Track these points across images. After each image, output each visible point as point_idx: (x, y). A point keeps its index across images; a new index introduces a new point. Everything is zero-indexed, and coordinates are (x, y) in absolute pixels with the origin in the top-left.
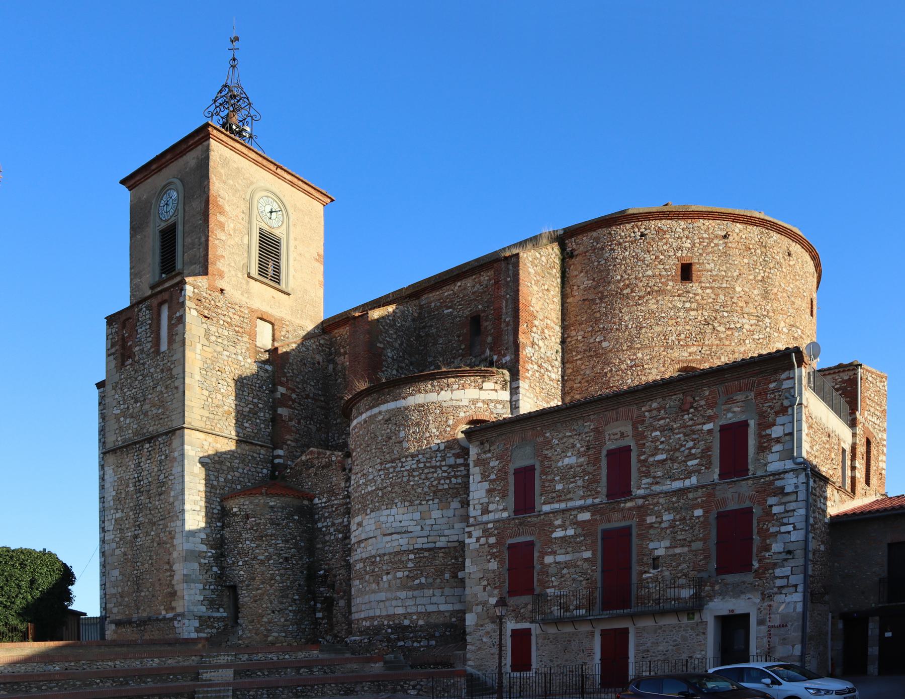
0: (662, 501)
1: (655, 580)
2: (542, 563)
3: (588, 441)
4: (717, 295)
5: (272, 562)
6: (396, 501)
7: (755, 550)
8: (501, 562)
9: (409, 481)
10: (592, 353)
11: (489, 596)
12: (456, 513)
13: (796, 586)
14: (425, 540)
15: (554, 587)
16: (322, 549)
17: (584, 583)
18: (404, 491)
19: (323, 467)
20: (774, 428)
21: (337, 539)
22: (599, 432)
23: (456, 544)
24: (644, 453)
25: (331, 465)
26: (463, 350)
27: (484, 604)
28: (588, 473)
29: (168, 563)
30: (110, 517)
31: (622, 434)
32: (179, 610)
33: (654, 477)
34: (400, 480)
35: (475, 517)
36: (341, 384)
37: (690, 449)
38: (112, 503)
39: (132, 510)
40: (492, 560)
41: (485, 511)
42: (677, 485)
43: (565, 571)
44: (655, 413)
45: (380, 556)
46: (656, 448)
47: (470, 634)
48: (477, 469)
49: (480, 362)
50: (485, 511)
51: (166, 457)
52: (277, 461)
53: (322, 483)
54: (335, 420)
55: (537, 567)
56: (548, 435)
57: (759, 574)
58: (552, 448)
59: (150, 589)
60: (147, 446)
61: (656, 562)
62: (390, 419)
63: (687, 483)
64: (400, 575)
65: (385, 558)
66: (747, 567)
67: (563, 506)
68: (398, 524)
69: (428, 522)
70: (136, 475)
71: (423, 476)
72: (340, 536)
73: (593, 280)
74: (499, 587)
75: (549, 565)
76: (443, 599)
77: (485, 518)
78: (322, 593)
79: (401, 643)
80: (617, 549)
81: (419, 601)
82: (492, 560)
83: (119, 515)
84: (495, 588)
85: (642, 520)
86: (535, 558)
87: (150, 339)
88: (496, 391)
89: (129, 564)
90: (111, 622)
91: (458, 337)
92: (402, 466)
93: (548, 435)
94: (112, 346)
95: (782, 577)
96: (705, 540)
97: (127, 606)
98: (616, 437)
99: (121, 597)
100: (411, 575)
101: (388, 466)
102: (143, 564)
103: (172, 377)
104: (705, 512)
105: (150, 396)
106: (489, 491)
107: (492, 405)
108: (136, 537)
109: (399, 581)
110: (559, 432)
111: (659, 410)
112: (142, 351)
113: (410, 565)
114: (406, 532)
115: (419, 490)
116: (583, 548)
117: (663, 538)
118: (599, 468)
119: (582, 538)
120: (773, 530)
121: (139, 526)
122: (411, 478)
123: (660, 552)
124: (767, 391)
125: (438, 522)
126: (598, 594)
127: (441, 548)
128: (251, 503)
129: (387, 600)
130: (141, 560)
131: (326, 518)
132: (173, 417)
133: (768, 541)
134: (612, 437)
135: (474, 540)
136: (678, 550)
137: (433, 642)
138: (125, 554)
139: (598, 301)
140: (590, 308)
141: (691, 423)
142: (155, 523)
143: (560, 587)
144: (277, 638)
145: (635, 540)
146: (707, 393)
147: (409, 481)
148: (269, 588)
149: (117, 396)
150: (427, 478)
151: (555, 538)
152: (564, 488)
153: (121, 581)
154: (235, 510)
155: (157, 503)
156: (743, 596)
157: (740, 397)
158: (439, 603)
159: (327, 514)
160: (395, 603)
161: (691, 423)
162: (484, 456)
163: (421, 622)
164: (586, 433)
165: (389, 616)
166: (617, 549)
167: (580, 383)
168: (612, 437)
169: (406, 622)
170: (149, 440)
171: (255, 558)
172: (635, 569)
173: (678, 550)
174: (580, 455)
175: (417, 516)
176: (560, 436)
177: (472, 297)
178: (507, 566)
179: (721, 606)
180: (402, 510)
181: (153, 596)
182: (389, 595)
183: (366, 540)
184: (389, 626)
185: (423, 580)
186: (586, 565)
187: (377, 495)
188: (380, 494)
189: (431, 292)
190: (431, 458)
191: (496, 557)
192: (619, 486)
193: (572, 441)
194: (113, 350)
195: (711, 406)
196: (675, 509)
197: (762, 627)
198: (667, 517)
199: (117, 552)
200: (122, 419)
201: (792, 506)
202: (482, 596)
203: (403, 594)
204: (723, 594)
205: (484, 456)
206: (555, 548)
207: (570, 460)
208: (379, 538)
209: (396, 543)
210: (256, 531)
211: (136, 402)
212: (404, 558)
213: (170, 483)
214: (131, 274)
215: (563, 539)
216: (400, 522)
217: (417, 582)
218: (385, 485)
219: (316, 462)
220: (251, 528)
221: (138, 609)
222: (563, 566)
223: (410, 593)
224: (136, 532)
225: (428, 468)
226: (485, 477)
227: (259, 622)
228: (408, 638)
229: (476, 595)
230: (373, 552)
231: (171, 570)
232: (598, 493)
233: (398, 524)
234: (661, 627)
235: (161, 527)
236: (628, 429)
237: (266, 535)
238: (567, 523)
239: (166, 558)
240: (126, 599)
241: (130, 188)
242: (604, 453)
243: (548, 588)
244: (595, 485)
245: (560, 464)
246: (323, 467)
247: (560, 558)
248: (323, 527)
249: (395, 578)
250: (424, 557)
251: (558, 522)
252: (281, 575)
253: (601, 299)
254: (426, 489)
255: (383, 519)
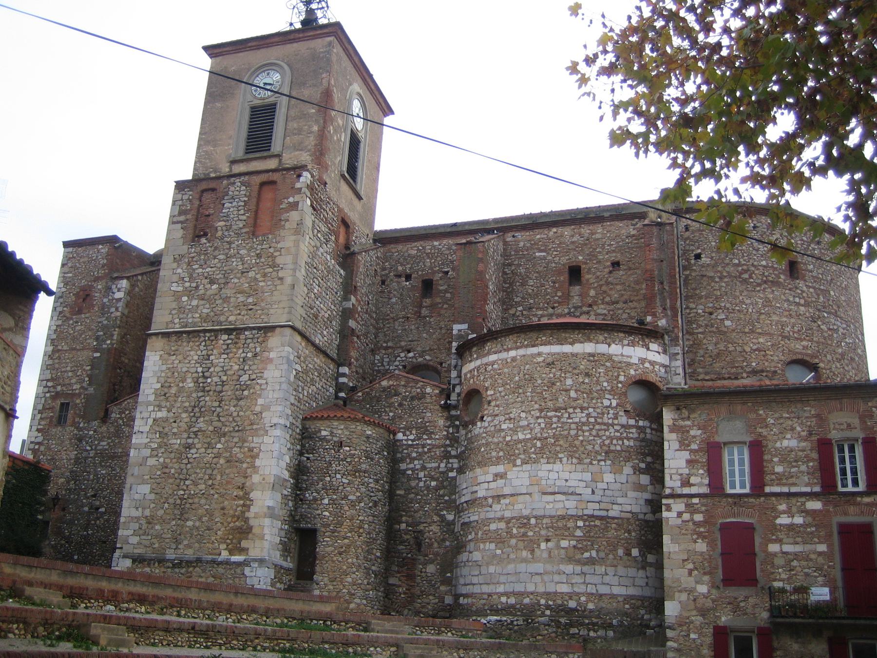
2: (765, 551)
3: (810, 426)
4: (818, 295)
5: (362, 504)
6: (560, 455)
8: (711, 544)
9: (577, 436)
10: (714, 329)
11: (697, 582)
12: (629, 480)
14: (597, 506)
21: (428, 487)
23: (629, 515)
26: (559, 297)
29: (242, 487)
30: (146, 415)
31: (849, 425)
32: (254, 553)
35: (672, 488)
38: (152, 398)
39: (186, 412)
40: (700, 541)
43: (795, 563)
45: (535, 517)
49: (581, 314)
50: (686, 483)
51: (255, 355)
53: (410, 416)
56: (761, 412)
59: (205, 519)
62: (553, 363)
64: (564, 543)
65: (545, 521)
67: (785, 489)
68: (564, 483)
69: (601, 485)
70: (200, 370)
71: (594, 432)
72: (433, 483)
73: (712, 258)
74: (709, 573)
75: (775, 555)
79: (575, 630)
81: (589, 579)
82: (700, 541)
84: (705, 574)
87: (244, 218)
88: (659, 353)
91: (554, 282)
92: (569, 418)
94: (181, 213)
97: (159, 536)
98: (842, 427)
99: (149, 523)
100: (580, 546)
101: (549, 414)
102: (196, 484)
105: (236, 281)
106: (689, 462)
108: (189, 447)
109: (563, 551)
110: (775, 411)
112: (229, 228)
113: (579, 533)
115: (590, 447)
116: (816, 540)
119: (813, 529)
122: (580, 433)
127: (613, 518)
129: (546, 573)
132: (272, 311)
134: (837, 426)
135: (674, 514)
139: (717, 280)
140: (709, 284)
147: (577, 436)
148: (357, 538)
149: (179, 271)
150: (598, 436)
151: (781, 525)
152: (784, 472)
154: (324, 433)
155: (233, 409)
159: (414, 455)
160: (557, 578)
162: (681, 423)
163: (591, 606)
164: (807, 417)
167: (703, 356)
168: (837, 426)
169: (572, 604)
170: (228, 331)
174: (801, 439)
175: (588, 476)
176: (776, 415)
178: (719, 550)
182: (549, 567)
183: (512, 495)
184: (548, 607)
186: (821, 560)
187: (535, 446)
190: (603, 414)
193: (790, 423)
194: (182, 218)
199: (152, 462)
200: (185, 299)
202: (688, 582)
203: (569, 568)
205: (681, 423)
208: (536, 496)
209: (561, 505)
210: (350, 463)
211: (212, 282)
212: (570, 524)
214: (200, 139)
215: (791, 527)
216: (566, 480)
217: (587, 555)
218: (545, 435)
220: (344, 459)
221: (177, 542)
223: (578, 569)
224: (190, 441)
225: (599, 424)
226: (684, 445)
228: (582, 624)
229: (678, 580)
230: (526, 512)
231: (246, 497)
233: (564, 483)
235: (236, 440)
237: (359, 471)
238: (794, 509)
240: (158, 527)
241: (211, 56)
243: (775, 580)
245: (778, 445)
246: (412, 398)
247: (787, 548)
248: (407, 469)
249: (558, 547)
250: (595, 526)
253: (721, 278)
254: (597, 448)
255: (540, 474)
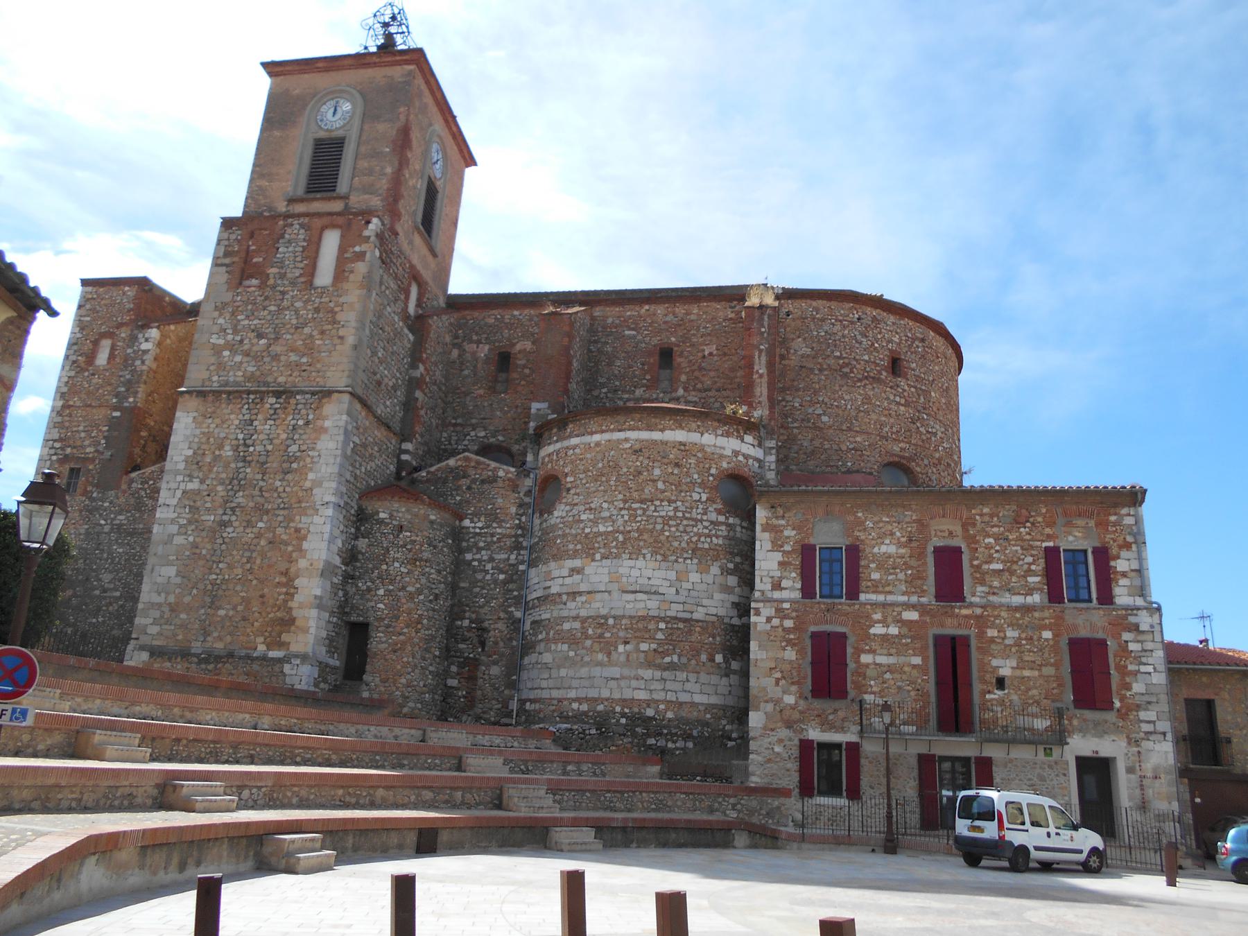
0: (1003, 614)
1: (1001, 702)
7: (1114, 687)
8: (801, 652)
9: (663, 530)
11: (784, 692)
13: (1164, 734)
14: (680, 607)
15: (874, 693)
16: (469, 590)
17: (913, 693)
18: (655, 541)
19: (483, 482)
20: (1119, 561)
21: (495, 581)
22: (923, 525)
23: (715, 619)
24: (977, 558)
25: (495, 481)
27: (777, 702)
28: (911, 568)
29: (286, 573)
30: (173, 485)
31: (951, 533)
32: (294, 648)
33: (991, 587)
34: (651, 527)
35: (763, 592)
36: (467, 377)
37: (1030, 564)
38: (181, 466)
39: (222, 484)
41: (777, 586)
42: (1017, 600)
43: (888, 676)
44: (987, 519)
45: (614, 617)
46: (991, 556)
47: (753, 739)
48: (766, 535)
50: (777, 586)
51: (307, 423)
52: (405, 457)
54: (455, 418)
55: (851, 665)
56: (860, 514)
57: (1123, 715)
58: (865, 530)
59: (240, 608)
60: (272, 400)
61: (1001, 683)
63: (1029, 599)
64: (644, 647)
65: (624, 622)
66: (1109, 706)
67: (881, 598)
68: (646, 581)
69: (685, 585)
70: (241, 436)
71: (681, 528)
72: (502, 577)
75: (867, 666)
76: (697, 688)
77: (777, 595)
78: (461, 651)
79: (651, 741)
80: (952, 659)
81: (669, 685)
83: (194, 485)
84: (793, 683)
85: (981, 634)
86: (849, 655)
89: (201, 563)
90: (142, 648)
91: (643, 364)
92: (655, 511)
93: (860, 514)
94: (226, 254)
95: (1149, 722)
96: (1056, 665)
97: (183, 626)
99: (172, 610)
101: (634, 506)
102: (231, 567)
103: (335, 322)
104: (1055, 635)
107: (751, 461)
109: (642, 655)
111: (992, 516)
113: (660, 636)
114: (656, 593)
115: (676, 544)
117: (1008, 657)
118: (925, 564)
120: (1131, 667)
121: (233, 509)
123: (1005, 672)
124: (1107, 523)
125: (697, 587)
126: (932, 710)
127: (698, 621)
128: (408, 511)
129: (623, 678)
130: (228, 559)
131: (479, 549)
132: (329, 374)
133: (1128, 679)
136: (1027, 673)
137: (690, 745)
138: (195, 545)
141: (1028, 537)
142: (267, 512)
143: (881, 694)
144: (413, 709)
145: (975, 655)
146: (1044, 511)
147: (663, 530)
149: (221, 321)
150: (685, 531)
153: (179, 586)
154: (382, 515)
155: (278, 483)
156: (1106, 737)
157: (1080, 522)
158: (698, 691)
159: (482, 544)
160: (634, 683)
161: (1028, 537)
162: (775, 522)
163: (670, 715)
165: (625, 700)
166: (952, 659)
169: (650, 712)
171: (403, 588)
172: (977, 687)
173: (1027, 673)
174: (900, 545)
175: (672, 575)
177: (663, 326)
179: (1081, 745)
180: (652, 564)
181: (244, 619)
182: (626, 672)
183: (589, 593)
184: (623, 715)
185: (675, 658)
187: (616, 539)
188: (621, 538)
189: (607, 305)
190: (692, 508)
191: (794, 645)
192: (950, 586)
194: (227, 261)
195: (1051, 524)
196: (1019, 627)
197: (1133, 776)
198: (1012, 634)
199: (179, 540)
201: (1149, 646)
202: (774, 692)
203: (647, 673)
204: (1083, 731)
206: (874, 646)
207: (888, 548)
208: (616, 595)
212: (652, 626)
213: (308, 460)
214: (253, 172)
217: (668, 659)
219: (471, 472)
220: (404, 546)
222: (885, 669)
223: (658, 674)
226: (776, 546)
227: (395, 682)
229: (765, 689)
232: (923, 591)
233: (646, 581)
234: (1011, 761)
235: (280, 518)
236: (958, 529)
237: (421, 560)
238: (890, 619)
239: (283, 566)
241: (271, 74)
242: (930, 549)
244: (920, 582)
245: (876, 550)
246: (483, 482)
247: (882, 659)
248: (474, 560)
249: (638, 650)
250: (678, 629)
251: (877, 616)
252: (429, 619)
254: (684, 545)
255: (621, 570)
